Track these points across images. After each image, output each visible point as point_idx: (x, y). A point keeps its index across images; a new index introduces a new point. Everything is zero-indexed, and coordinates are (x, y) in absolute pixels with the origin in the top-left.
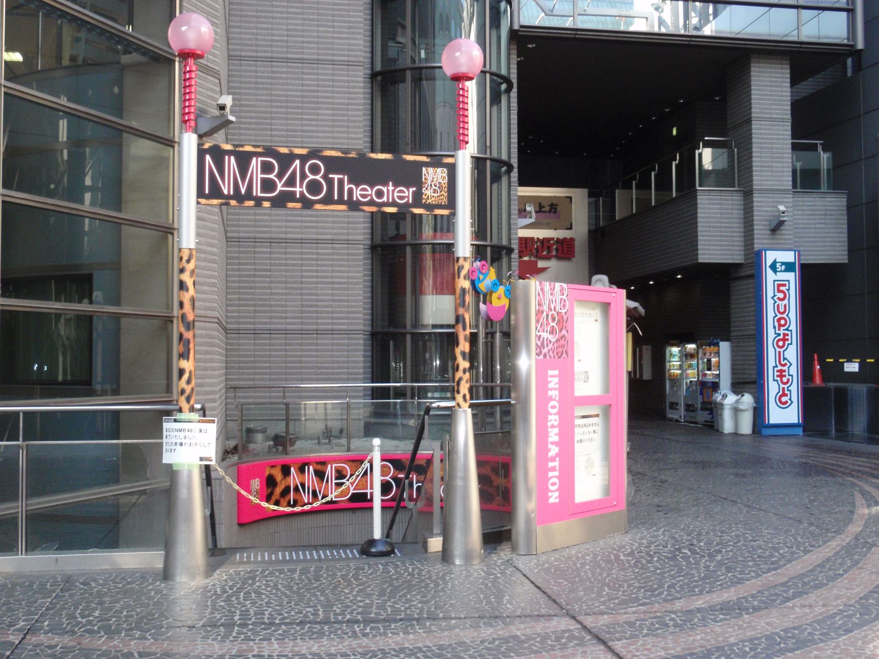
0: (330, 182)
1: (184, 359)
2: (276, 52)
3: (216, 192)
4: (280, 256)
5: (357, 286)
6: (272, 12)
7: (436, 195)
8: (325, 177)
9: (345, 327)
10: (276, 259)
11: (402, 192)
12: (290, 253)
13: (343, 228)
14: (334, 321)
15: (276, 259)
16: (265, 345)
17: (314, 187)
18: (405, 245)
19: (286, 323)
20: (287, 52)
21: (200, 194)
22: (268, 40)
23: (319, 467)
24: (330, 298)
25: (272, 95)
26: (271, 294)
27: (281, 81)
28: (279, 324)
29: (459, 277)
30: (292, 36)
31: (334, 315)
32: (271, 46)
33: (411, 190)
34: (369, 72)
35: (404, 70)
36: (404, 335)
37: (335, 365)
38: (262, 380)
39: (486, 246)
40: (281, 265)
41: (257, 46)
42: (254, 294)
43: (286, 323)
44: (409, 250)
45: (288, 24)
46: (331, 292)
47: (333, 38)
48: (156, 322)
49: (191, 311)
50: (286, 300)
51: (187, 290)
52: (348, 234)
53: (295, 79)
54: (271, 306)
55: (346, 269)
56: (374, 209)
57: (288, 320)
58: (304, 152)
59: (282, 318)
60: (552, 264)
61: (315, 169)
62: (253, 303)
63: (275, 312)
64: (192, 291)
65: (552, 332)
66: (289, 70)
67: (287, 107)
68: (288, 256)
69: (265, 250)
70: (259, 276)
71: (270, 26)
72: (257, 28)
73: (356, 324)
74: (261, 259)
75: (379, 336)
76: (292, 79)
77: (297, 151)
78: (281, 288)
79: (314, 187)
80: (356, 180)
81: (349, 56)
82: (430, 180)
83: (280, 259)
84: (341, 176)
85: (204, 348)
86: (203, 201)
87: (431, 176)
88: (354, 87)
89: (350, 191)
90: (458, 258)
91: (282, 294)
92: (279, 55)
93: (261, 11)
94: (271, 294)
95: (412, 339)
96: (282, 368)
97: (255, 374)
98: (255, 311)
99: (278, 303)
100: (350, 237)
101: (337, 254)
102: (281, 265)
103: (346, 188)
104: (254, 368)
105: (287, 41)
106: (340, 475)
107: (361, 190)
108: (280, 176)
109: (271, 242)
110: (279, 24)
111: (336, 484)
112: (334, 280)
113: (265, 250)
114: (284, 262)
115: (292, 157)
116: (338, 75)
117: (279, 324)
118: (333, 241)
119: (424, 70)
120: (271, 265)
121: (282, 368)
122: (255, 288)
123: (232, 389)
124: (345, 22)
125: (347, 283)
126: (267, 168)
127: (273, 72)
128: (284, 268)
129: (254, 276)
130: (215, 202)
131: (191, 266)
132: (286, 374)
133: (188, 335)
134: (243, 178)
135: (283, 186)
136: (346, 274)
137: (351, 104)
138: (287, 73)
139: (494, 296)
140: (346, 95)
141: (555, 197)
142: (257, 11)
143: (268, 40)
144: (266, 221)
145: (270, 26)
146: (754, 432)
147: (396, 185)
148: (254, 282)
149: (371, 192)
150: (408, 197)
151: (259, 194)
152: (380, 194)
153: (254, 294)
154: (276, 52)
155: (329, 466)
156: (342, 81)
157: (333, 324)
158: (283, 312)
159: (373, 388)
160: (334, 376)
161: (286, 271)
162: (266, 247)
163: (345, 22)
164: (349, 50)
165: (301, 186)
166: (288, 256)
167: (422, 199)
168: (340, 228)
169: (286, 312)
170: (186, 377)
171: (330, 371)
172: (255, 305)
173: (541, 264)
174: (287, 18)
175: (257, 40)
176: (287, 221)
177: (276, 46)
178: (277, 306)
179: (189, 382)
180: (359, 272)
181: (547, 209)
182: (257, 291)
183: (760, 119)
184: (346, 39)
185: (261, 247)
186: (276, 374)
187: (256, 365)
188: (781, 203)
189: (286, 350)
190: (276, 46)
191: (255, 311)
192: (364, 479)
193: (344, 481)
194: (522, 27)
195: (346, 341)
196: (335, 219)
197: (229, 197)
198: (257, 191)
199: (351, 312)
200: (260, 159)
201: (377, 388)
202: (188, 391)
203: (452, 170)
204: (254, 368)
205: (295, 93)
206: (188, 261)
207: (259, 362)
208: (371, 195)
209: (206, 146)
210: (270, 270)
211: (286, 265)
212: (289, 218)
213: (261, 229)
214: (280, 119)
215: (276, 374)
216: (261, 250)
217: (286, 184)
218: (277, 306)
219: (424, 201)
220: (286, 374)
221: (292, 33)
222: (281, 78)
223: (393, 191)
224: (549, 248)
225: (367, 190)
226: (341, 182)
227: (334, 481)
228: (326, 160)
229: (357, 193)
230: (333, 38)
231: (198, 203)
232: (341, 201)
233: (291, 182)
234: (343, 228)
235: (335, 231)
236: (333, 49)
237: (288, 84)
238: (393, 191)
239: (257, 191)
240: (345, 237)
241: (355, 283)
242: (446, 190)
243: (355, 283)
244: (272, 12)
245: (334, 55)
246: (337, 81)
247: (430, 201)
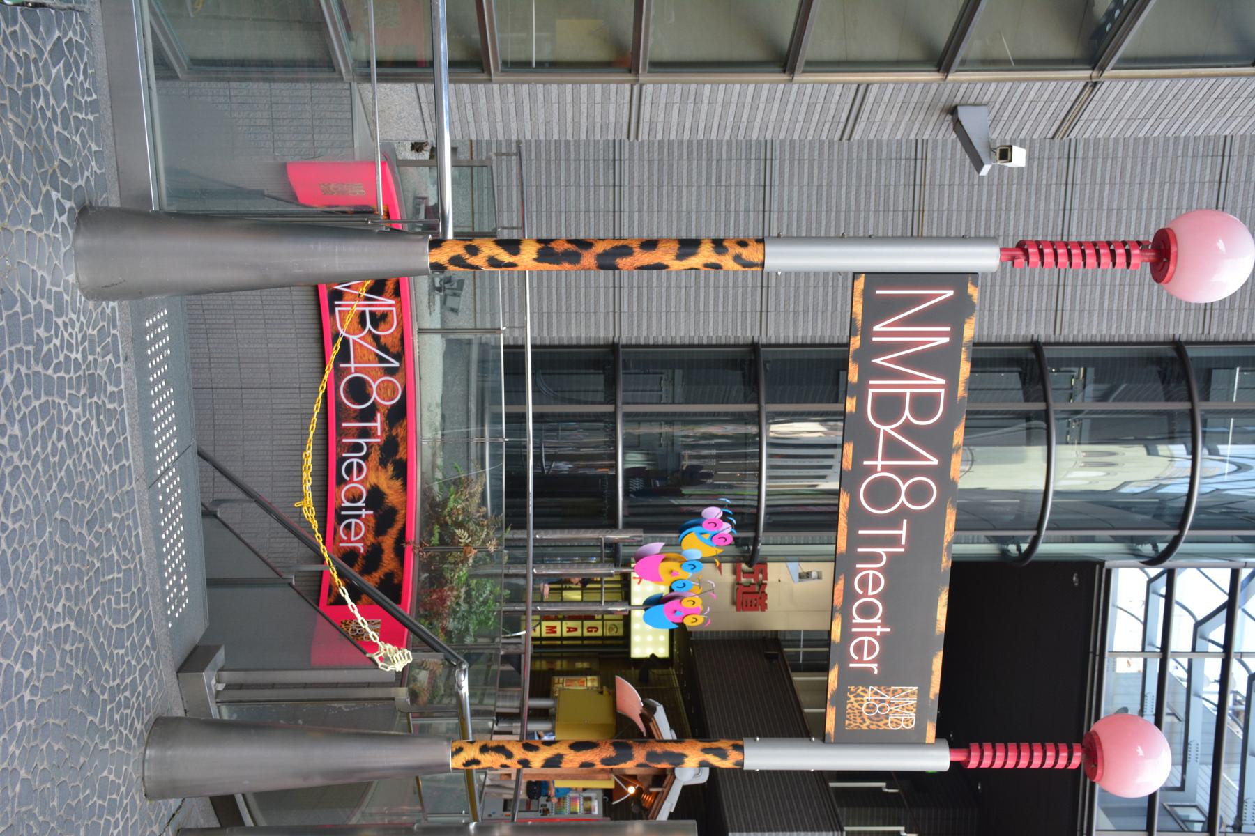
0: (893, 521)
1: (540, 252)
2: (1083, 190)
3: (877, 309)
4: (742, 202)
5: (692, 326)
6: (1152, 183)
7: (863, 709)
8: (903, 511)
9: (625, 308)
10: (737, 195)
11: (871, 652)
12: (747, 217)
13: (787, 304)
14: (635, 290)
15: (737, 195)
16: (596, 178)
18: (759, 403)
19: (631, 213)
20: (1081, 210)
21: (876, 278)
22: (1103, 177)
23: (390, 286)
24: (673, 284)
25: (1010, 185)
26: (680, 187)
27: (1033, 199)
28: (631, 199)
29: (706, 751)
30: (1108, 217)
31: (645, 290)
32: (1093, 183)
33: (874, 666)
34: (1043, 340)
35: (1046, 400)
36: (612, 400)
37: (564, 291)
38: (538, 172)
39: (756, 530)
40: (728, 203)
41: (1095, 158)
42: (680, 158)
43: (631, 213)
44: (752, 407)
45: (1129, 209)
46: (683, 284)
47: (1103, 285)
49: (638, 264)
50: (670, 212)
51: (680, 257)
52: (777, 312)
53: (1036, 222)
54: (660, 186)
55: (721, 309)
56: (836, 635)
57: (636, 214)
59: (641, 203)
61: (918, 493)
62: (666, 157)
63: (651, 192)
64: (676, 265)
66: (1052, 214)
67: (988, 210)
68: (742, 214)
69: (753, 177)
70: (709, 167)
71: (1127, 180)
72: (1125, 158)
73: (631, 324)
74: (738, 171)
75: (612, 358)
76: (1036, 218)
78: (689, 202)
80: (893, 568)
81: (1072, 310)
82: (894, 699)
83: (737, 201)
84: (903, 542)
85: (584, 120)
86: (860, 284)
87: (902, 700)
88: (1019, 320)
89: (875, 558)
90: (739, 748)
91: (679, 205)
92: (1077, 195)
93: (1154, 165)
94: (680, 187)
95: (604, 414)
96: (558, 204)
97: (548, 162)
98: (650, 161)
99: (665, 199)
100: (772, 315)
101: (744, 294)
102: (728, 203)
103: (880, 551)
104: (558, 159)
105: (1100, 208)
106: (379, 319)
107: (876, 579)
108: (907, 429)
110: (1130, 195)
111: (364, 312)
112: (702, 290)
113: (753, 177)
114: (732, 208)
116: (1040, 293)
117: (631, 199)
119: (1044, 425)
120: (728, 186)
121: (558, 204)
122: (690, 160)
123: (518, 151)
124: (1130, 304)
125: (698, 312)
126: (924, 405)
127: (1048, 186)
128: (723, 208)
129: (709, 159)
130: (858, 308)
131: (727, 262)
132: (549, 211)
133: (588, 259)
134: (901, 361)
135: (885, 432)
136: (711, 309)
137: (991, 316)
138: (1047, 211)
139: (674, 566)
140: (1006, 308)
142: (1154, 158)
143: (1103, 177)
144: (800, 178)
145: (1127, 180)
147: (883, 639)
148: (699, 159)
149: (872, 596)
150: (860, 661)
151: (871, 391)
152: (867, 611)
153: (680, 158)
154: (1083, 190)
155: (393, 302)
157: (631, 288)
158: (650, 206)
159: (523, 347)
160: (545, 290)
161: (718, 211)
162: (757, 178)
163: (1130, 304)
164: (1082, 311)
165: (884, 468)
166: (742, 214)
167: (857, 686)
168: (787, 299)
169: (651, 211)
170: (504, 257)
171: (554, 284)
172: (660, 160)
174: (1139, 209)
175: (1105, 159)
176: (799, 212)
177: (1092, 192)
178: (660, 196)
179: (493, 262)
180: (716, 330)
182: (685, 163)
184: (1102, 304)
185: (758, 170)
186: (548, 195)
187: (563, 163)
189: (587, 211)
190: (1092, 192)
191: (650, 161)
192: (372, 357)
193: (369, 326)
194: (1109, 572)
195: (602, 309)
196: (801, 291)
197: (867, 333)
198: (877, 387)
199: (649, 318)
200: (942, 391)
201: (523, 355)
202: (472, 260)
204: (558, 159)
205: (1012, 223)
206: (737, 258)
207: (568, 169)
208: (865, 595)
209: (973, 291)
210: (718, 184)
211: (728, 211)
212: (804, 216)
213: (787, 170)
214: (970, 199)
215: (548, 195)
216: (753, 170)
217: (889, 439)
218: (660, 196)
219: (852, 688)
220: (549, 211)
221: (1114, 218)
222: (1038, 200)
223: (873, 635)
225: (875, 587)
226: (894, 541)
227: (367, 310)
228: (937, 513)
230: (1103, 285)
231: (855, 275)
233: (894, 449)
234: (787, 304)
235: (782, 291)
236: (1084, 285)
237: (1028, 210)
238: (873, 635)
239: (877, 387)
240: (772, 308)
241: (697, 323)
242: (874, 727)
243: (697, 323)
244: (1152, 183)
245: (1074, 287)
246: (1030, 292)
247: (853, 699)
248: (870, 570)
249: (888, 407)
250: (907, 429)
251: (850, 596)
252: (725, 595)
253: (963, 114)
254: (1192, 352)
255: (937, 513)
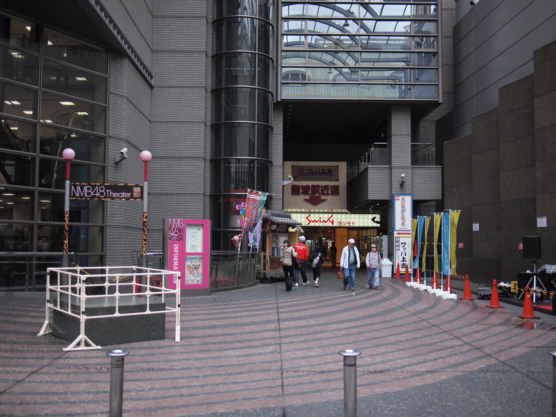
0: (106, 192)
17: (102, 194)
21: (70, 196)
48: (100, 228)
58: (99, 184)
60: (330, 198)
61: (102, 189)
65: (176, 233)
77: (97, 184)
79: (102, 194)
108: (92, 191)
109: (166, 194)
115: (96, 186)
118: (191, 194)
126: (88, 189)
141: (331, 166)
146: (392, 277)
149: (118, 195)
156: (196, 130)
173: (323, 197)
181: (327, 171)
183: (396, 135)
188: (403, 173)
197: (78, 197)
198: (86, 195)
203: (142, 188)
214: (171, 145)
224: (327, 190)
226: (109, 192)
228: (105, 186)
229: (114, 195)
232: (109, 197)
233: (95, 192)
239: (86, 195)
248: (114, 195)
249: (89, 194)
250: (92, 191)
251: (118, 198)
252: (335, 197)
253: (116, 161)
254: (214, 88)
255: (105, 186)
